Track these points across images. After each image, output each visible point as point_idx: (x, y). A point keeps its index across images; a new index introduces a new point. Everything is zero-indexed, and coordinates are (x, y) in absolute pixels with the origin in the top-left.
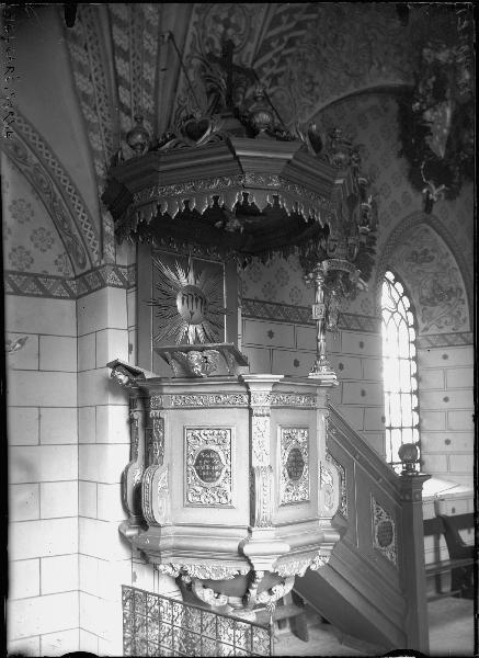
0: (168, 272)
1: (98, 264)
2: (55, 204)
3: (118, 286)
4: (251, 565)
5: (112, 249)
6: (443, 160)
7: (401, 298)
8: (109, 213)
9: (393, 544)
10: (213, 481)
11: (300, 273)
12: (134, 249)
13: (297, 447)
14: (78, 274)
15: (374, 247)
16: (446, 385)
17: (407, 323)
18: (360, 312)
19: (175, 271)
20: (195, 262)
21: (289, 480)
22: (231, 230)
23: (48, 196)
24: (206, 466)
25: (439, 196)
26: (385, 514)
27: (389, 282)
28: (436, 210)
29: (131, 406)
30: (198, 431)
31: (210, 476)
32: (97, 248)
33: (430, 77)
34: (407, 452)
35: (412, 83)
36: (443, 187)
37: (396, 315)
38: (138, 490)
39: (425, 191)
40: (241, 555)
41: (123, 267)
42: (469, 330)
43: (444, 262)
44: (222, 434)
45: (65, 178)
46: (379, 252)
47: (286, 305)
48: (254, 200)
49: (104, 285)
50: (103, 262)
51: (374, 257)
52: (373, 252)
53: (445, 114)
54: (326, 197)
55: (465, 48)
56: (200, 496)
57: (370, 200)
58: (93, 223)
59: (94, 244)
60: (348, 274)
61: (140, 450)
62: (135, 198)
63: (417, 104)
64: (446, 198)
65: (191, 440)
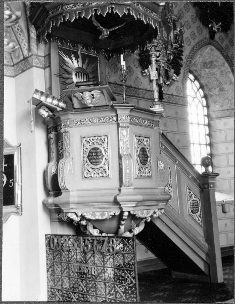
0: (67, 59)
1: (27, 55)
4: (121, 208)
5: (35, 46)
7: (198, 90)
8: (33, 26)
9: (199, 213)
10: (97, 165)
11: (139, 69)
12: (48, 45)
13: (143, 147)
14: (15, 63)
15: (182, 57)
16: (226, 140)
18: (175, 93)
19: (71, 58)
20: (83, 55)
21: (140, 164)
24: (94, 156)
25: (218, 29)
26: (193, 195)
28: (217, 36)
29: (48, 132)
30: (89, 139)
31: (96, 162)
32: (26, 47)
34: (206, 162)
37: (196, 99)
38: (55, 178)
39: (210, 26)
40: (116, 202)
41: (41, 56)
42: (219, 222)
43: (223, 69)
44: (102, 139)
46: (185, 60)
47: (132, 87)
48: (116, 11)
49: (32, 67)
50: (30, 54)
51: (182, 62)
52: (182, 59)
54: (155, 12)
55: (173, 271)
56: (91, 174)
57: (178, 29)
58: (23, 34)
59: (25, 45)
60: (168, 70)
61: (54, 155)
62: (50, 13)
64: (222, 31)
65: (85, 143)
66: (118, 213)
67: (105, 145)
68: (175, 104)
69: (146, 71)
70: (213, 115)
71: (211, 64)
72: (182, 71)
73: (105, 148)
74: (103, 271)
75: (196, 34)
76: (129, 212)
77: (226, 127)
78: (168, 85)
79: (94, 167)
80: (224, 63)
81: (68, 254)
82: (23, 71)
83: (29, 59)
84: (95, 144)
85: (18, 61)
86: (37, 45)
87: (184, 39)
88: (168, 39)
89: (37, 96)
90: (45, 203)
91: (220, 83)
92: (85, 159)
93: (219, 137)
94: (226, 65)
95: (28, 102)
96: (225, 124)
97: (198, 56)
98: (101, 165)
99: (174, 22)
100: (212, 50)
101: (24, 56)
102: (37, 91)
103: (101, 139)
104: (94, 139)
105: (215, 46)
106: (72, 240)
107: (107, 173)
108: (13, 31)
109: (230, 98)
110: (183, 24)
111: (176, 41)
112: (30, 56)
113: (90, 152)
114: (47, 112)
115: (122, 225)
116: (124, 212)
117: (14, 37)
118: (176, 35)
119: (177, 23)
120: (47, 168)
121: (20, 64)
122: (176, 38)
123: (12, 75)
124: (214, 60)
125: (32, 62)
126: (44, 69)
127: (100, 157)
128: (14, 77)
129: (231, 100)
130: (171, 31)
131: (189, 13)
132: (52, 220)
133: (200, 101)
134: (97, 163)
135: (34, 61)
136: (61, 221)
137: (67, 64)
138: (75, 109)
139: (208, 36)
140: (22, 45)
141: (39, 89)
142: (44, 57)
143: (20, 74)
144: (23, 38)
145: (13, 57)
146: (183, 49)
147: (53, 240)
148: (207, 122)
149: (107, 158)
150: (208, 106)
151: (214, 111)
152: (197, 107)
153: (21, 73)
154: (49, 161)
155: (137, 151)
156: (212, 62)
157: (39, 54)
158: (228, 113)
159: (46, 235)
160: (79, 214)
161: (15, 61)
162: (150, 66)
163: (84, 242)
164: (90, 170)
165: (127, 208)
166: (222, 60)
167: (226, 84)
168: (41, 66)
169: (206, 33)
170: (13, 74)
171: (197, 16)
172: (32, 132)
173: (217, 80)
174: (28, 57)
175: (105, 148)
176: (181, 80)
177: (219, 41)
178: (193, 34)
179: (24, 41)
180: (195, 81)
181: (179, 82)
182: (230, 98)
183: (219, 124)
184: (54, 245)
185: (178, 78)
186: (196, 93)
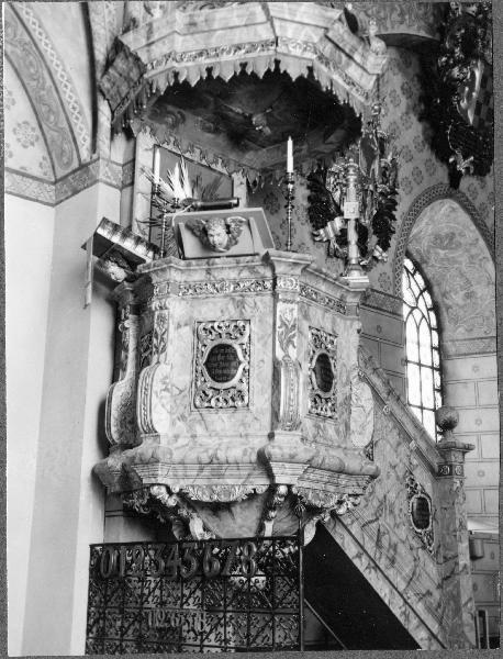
1: (88, 160)
2: (42, 92)
3: (111, 185)
4: (271, 476)
6: (472, 128)
11: (308, 228)
13: (325, 352)
14: (58, 177)
15: (394, 212)
16: (476, 387)
17: (429, 325)
22: (238, 92)
23: (35, 83)
24: (219, 362)
25: (467, 169)
27: (408, 271)
28: (465, 183)
30: (210, 325)
33: (459, 30)
35: (437, 37)
36: (472, 158)
37: (416, 312)
39: (451, 160)
41: (117, 164)
43: (474, 251)
45: (40, 30)
46: (399, 222)
49: (96, 181)
52: (393, 218)
53: (473, 75)
56: (209, 401)
63: (444, 59)
65: (202, 333)
66: (261, 490)
67: (245, 340)
68: (377, 308)
69: (322, 231)
70: (451, 348)
71: (451, 239)
72: (393, 242)
73: (244, 347)
74: (222, 621)
75: (424, 173)
76: (289, 487)
77: (475, 376)
78: (364, 266)
79: (218, 385)
80: (477, 240)
81: (142, 588)
82: (76, 192)
83: (90, 167)
84: (224, 336)
85: (67, 172)
86: (112, 139)
87: (399, 179)
88: (368, 173)
89: (103, 233)
90: (96, 471)
91: (468, 281)
92: (199, 368)
93: (462, 396)
94: (482, 242)
95: (84, 247)
96: (476, 369)
97: (426, 220)
98: (234, 381)
99: (382, 141)
100: (454, 210)
101: (80, 160)
102: (105, 221)
103: (236, 326)
104: (222, 325)
105: (460, 203)
106: (151, 552)
107: (246, 398)
108: (64, 110)
109: (487, 314)
110: (399, 150)
111: (385, 180)
112: (95, 161)
113: (212, 353)
114: (124, 268)
115: (269, 520)
116: (278, 485)
117: (65, 122)
118: (386, 168)
119: (387, 145)
120: (111, 393)
121: (70, 178)
122: (384, 174)
123: (51, 202)
124: (457, 232)
125: (98, 172)
126: (121, 190)
127: (234, 364)
128: (52, 205)
129: (488, 319)
130: (374, 158)
131: (410, 131)
132: (108, 515)
133: (424, 316)
134: (227, 378)
135: (102, 171)
136: (131, 515)
137: (164, 196)
138: (184, 259)
139: (446, 181)
140: (80, 140)
141: (110, 218)
142: (123, 166)
143: (67, 198)
144: (82, 126)
145: (56, 166)
146: (397, 198)
147: (108, 557)
148: (437, 362)
149: (247, 368)
150: (440, 329)
151: (453, 341)
152: (418, 328)
153: (73, 195)
154: (114, 379)
155: (312, 359)
156: (451, 236)
157: (113, 159)
158: (481, 345)
159: (92, 547)
160: (176, 489)
161: (61, 173)
162: (329, 223)
163: (182, 555)
164: (210, 393)
165: (284, 476)
166: (472, 232)
167: (478, 283)
168: (114, 182)
169: (442, 174)
170: (53, 200)
171: (426, 139)
172: (86, 305)
173: (462, 275)
174: (89, 164)
175: (244, 347)
176: (389, 260)
177: (468, 195)
178: (417, 173)
179: (85, 131)
180: (415, 272)
181: (387, 265)
182: (487, 314)
183: (462, 368)
184: (106, 572)
185: (384, 254)
186: (417, 299)
